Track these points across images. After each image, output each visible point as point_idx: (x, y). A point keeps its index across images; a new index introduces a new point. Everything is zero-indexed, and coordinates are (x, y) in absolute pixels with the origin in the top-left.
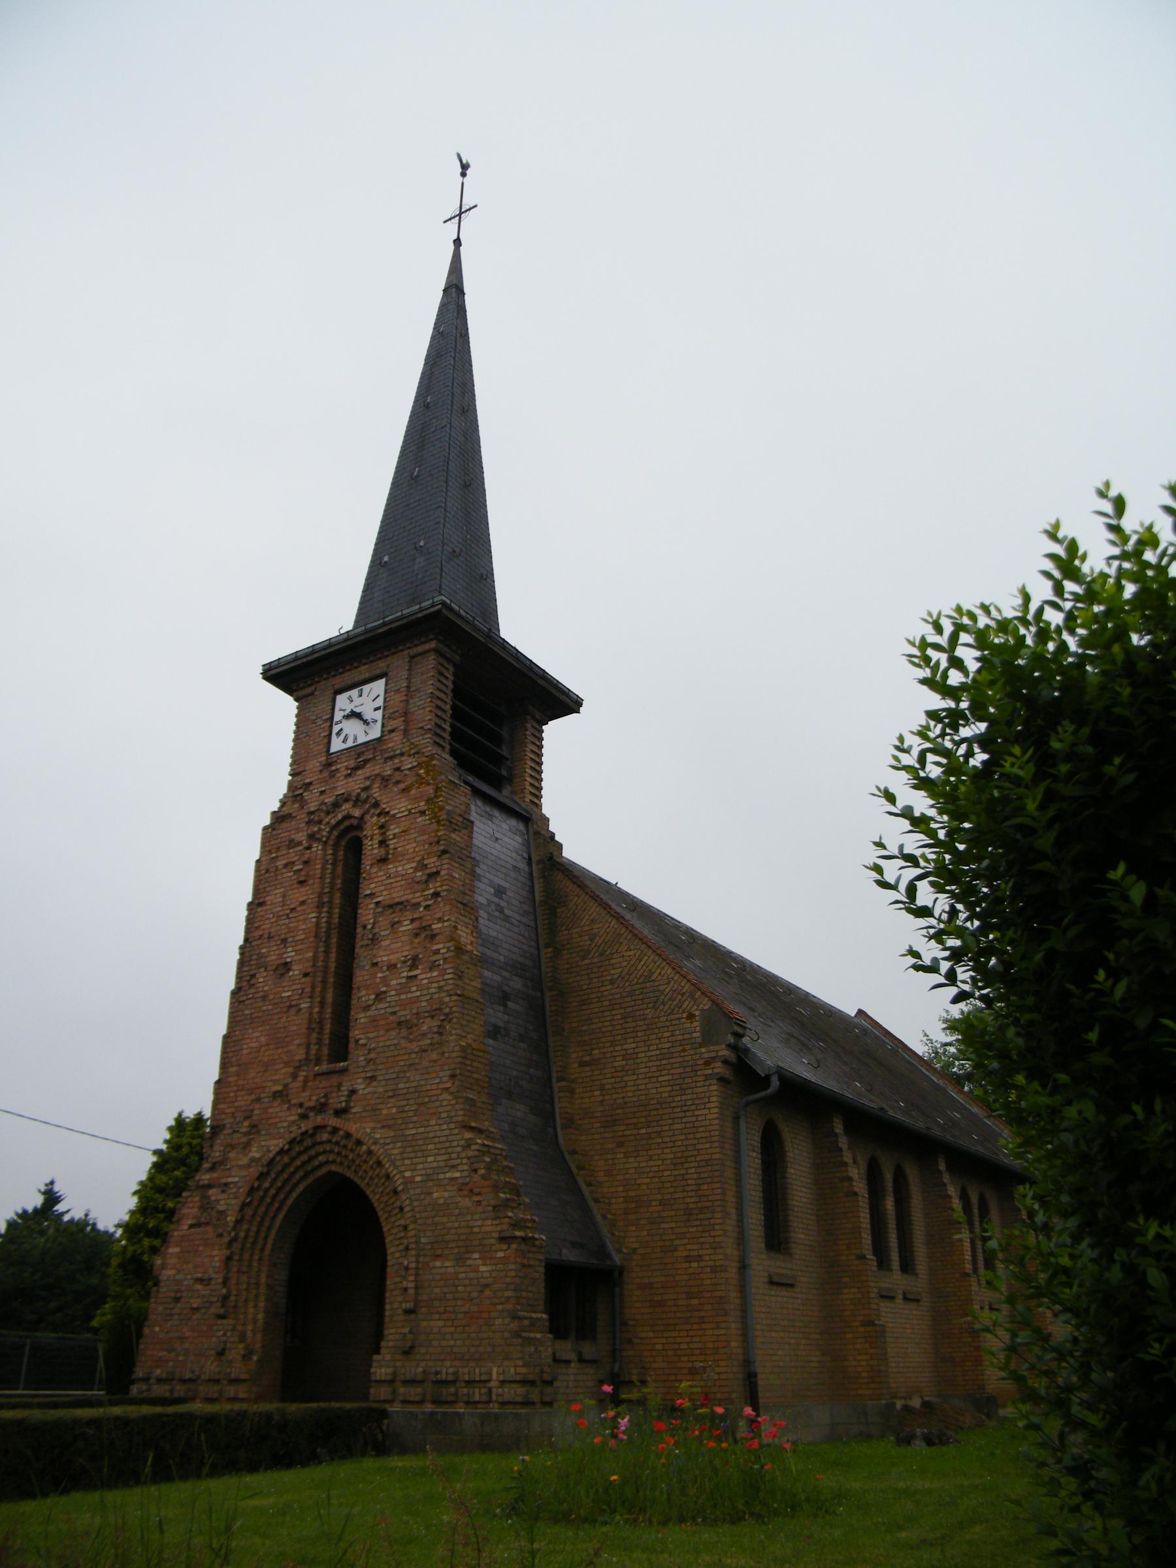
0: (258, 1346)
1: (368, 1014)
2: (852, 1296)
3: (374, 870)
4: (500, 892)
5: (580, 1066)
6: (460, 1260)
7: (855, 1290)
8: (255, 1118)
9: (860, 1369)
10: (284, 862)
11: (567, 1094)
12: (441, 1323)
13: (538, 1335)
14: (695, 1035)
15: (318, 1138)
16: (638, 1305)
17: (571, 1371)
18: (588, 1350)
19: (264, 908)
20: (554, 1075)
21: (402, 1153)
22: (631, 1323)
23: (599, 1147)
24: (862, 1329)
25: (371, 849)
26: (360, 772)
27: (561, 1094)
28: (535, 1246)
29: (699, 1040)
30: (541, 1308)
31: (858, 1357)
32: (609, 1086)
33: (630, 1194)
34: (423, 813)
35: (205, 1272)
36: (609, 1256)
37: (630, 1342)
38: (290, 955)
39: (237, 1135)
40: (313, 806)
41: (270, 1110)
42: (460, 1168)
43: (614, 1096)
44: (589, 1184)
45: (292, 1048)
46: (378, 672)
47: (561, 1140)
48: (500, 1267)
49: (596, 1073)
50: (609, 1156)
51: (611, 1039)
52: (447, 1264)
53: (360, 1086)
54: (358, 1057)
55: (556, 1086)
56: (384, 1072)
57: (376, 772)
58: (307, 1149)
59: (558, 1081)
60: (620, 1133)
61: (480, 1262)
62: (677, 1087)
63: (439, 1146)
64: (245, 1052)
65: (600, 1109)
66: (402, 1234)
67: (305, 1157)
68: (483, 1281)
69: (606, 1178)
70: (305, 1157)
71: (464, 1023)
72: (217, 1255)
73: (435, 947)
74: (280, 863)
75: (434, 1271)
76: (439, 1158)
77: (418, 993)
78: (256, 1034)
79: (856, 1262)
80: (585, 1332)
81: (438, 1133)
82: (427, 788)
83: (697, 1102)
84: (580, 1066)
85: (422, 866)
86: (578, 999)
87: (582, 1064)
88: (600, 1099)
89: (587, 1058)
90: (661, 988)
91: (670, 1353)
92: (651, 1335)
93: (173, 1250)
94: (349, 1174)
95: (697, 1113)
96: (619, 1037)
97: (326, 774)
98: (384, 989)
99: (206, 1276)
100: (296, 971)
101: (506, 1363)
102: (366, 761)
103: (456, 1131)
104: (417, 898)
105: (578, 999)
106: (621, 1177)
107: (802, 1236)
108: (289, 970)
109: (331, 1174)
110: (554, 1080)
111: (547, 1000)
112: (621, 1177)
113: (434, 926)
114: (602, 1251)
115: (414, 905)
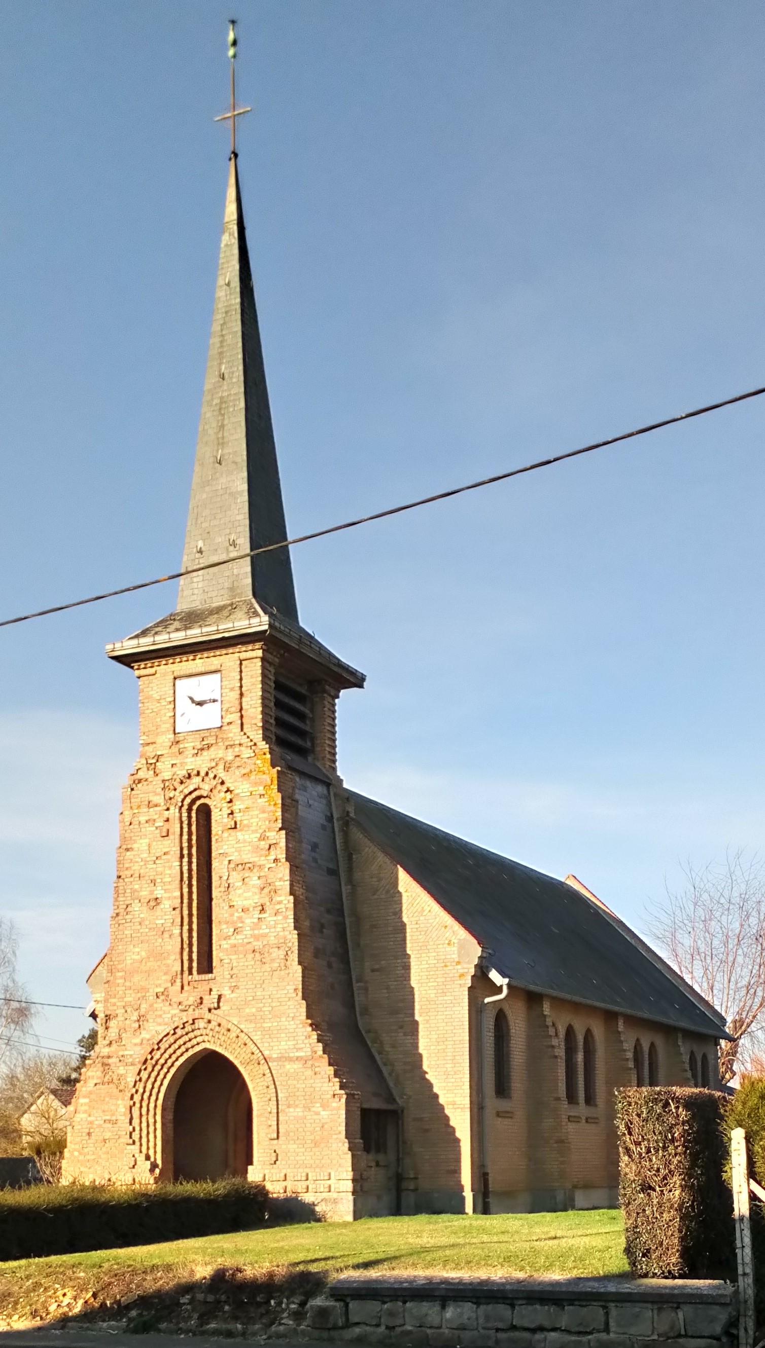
0: (159, 1162)
1: (229, 942)
3: (226, 835)
4: (315, 847)
6: (307, 1108)
10: (147, 818)
12: (295, 1146)
15: (196, 1026)
18: (381, 1157)
19: (133, 853)
20: (354, 977)
24: (555, 1145)
25: (219, 819)
26: (205, 753)
29: (457, 960)
30: (359, 1136)
33: (408, 1060)
34: (261, 796)
35: (113, 1115)
36: (394, 1100)
38: (159, 893)
40: (167, 775)
41: (155, 1005)
44: (380, 1053)
45: (169, 962)
46: (213, 668)
47: (360, 1024)
48: (335, 1112)
52: (298, 1110)
53: (226, 992)
55: (356, 985)
57: (220, 756)
66: (265, 1091)
67: (186, 1038)
68: (323, 1121)
70: (186, 1038)
72: (122, 1106)
73: (279, 899)
74: (143, 819)
76: (289, 1043)
77: (267, 931)
82: (264, 776)
85: (263, 838)
87: (373, 971)
89: (377, 967)
90: (431, 921)
93: (82, 1101)
97: (175, 749)
98: (240, 925)
99: (114, 1118)
100: (166, 905)
101: (340, 1169)
102: (209, 747)
104: (262, 861)
107: (519, 1085)
108: (158, 904)
109: (205, 1049)
110: (354, 982)
113: (277, 884)
114: (391, 1099)
115: (260, 866)
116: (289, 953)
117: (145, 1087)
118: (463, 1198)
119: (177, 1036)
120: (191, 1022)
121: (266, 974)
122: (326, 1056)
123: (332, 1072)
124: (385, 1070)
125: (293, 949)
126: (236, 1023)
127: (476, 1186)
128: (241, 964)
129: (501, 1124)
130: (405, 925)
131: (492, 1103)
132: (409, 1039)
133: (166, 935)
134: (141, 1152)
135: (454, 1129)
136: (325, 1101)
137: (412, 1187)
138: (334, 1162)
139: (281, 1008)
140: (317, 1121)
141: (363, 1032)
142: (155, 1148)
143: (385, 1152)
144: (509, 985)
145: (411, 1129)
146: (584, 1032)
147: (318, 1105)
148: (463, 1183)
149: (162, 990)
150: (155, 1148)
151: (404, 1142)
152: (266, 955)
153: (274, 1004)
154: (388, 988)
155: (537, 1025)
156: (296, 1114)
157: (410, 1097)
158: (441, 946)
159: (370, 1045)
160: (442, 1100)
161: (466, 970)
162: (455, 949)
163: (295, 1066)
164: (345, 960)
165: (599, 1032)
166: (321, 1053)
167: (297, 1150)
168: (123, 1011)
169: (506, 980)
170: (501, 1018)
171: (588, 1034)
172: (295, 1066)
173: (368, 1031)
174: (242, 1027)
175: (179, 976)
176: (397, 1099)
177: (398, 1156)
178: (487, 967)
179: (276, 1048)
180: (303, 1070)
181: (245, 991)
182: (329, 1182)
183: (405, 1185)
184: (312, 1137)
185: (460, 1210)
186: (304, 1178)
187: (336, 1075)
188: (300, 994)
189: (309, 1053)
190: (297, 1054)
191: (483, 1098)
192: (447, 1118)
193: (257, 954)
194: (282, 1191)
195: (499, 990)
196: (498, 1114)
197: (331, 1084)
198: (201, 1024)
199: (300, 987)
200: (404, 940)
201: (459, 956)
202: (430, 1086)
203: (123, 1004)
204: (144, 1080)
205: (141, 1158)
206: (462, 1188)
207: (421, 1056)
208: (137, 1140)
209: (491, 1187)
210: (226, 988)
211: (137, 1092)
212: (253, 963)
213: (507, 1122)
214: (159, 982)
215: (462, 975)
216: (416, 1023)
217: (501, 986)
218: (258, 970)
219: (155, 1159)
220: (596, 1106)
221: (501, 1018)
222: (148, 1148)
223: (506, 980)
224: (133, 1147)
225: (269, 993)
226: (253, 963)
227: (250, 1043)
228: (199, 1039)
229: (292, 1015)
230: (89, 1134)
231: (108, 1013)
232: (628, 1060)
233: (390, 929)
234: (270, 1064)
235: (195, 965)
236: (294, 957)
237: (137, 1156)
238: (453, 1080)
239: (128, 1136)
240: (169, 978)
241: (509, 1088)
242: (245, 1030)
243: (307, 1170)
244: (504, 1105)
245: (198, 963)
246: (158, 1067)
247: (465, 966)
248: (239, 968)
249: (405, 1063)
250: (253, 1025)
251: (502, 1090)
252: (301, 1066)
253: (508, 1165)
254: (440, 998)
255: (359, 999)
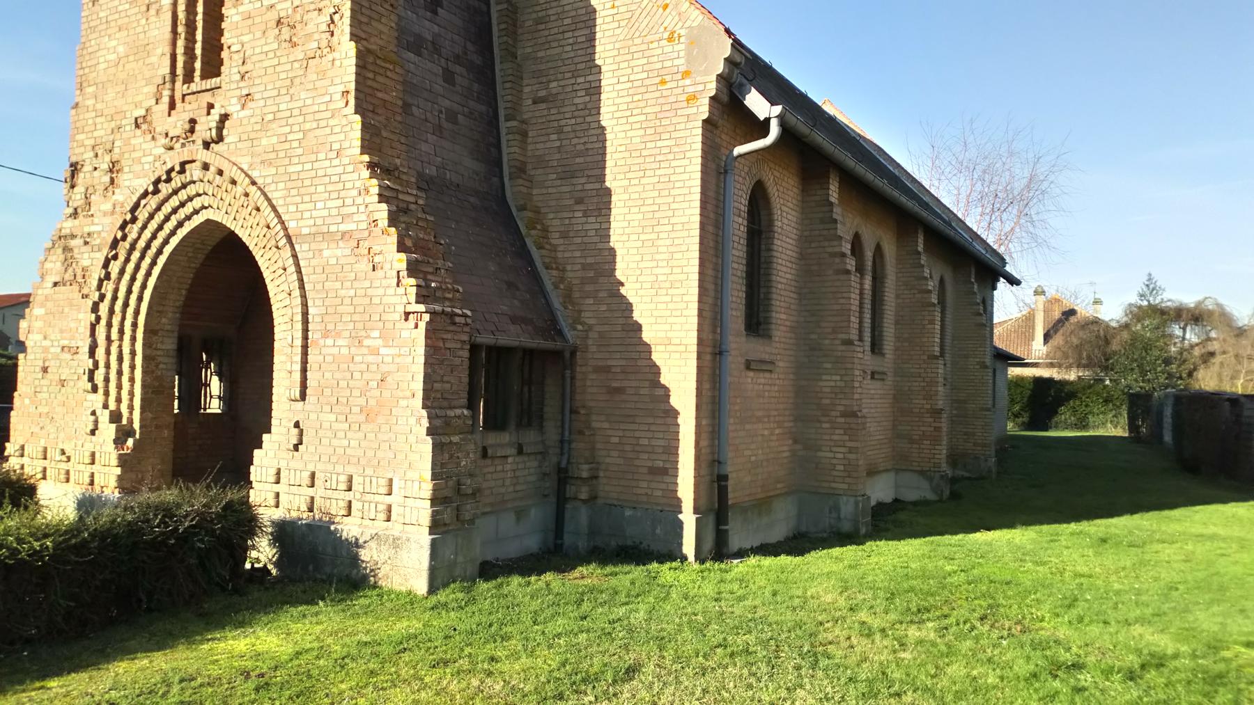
2: (833, 384)
5: (535, 103)
7: (838, 378)
8: (116, 150)
9: (834, 461)
11: (517, 137)
12: (332, 417)
13: (455, 439)
14: (676, 62)
16: (595, 390)
17: (508, 467)
18: (530, 437)
20: (502, 113)
21: (285, 198)
22: (582, 412)
23: (553, 203)
24: (842, 420)
27: (511, 137)
28: (455, 324)
29: (682, 69)
31: (834, 449)
32: (569, 129)
33: (589, 260)
35: (72, 338)
36: (560, 333)
37: (581, 433)
39: (96, 174)
41: (133, 141)
42: (356, 218)
43: (575, 141)
45: (154, 59)
49: (553, 111)
50: (565, 215)
51: (573, 67)
52: (340, 342)
53: (233, 108)
54: (230, 68)
55: (504, 126)
56: (262, 88)
58: (175, 192)
59: (507, 120)
60: (580, 187)
61: (380, 342)
62: (652, 131)
63: (330, 188)
64: (102, 66)
65: (557, 156)
69: (561, 241)
71: (364, 19)
75: (324, 351)
76: (330, 204)
78: (114, 43)
79: (843, 348)
80: (530, 417)
81: (329, 171)
83: (675, 149)
84: (535, 103)
86: (534, 16)
88: (558, 144)
89: (542, 93)
91: (628, 448)
92: (606, 425)
94: (231, 225)
95: (674, 163)
96: (582, 66)
99: (73, 344)
103: (350, 168)
105: (534, 16)
106: (579, 240)
107: (783, 316)
109: (208, 221)
110: (502, 118)
111: (494, 16)
112: (579, 240)
114: (552, 328)
116: (336, 17)
117: (116, 291)
118: (680, 524)
119: (161, 196)
120: (177, 168)
121: (296, 65)
122: (393, 229)
123: (404, 266)
124: (548, 278)
125: (343, 9)
126: (245, 167)
127: (703, 502)
128: (258, 50)
129: (753, 382)
130: (595, 11)
131: (739, 345)
132: (592, 224)
133: (152, 12)
134: (106, 406)
135: (666, 390)
136: (389, 325)
137: (583, 496)
138: (400, 456)
139: (318, 132)
140: (373, 368)
141: (514, 210)
142: (131, 400)
143: (541, 427)
144: (781, 117)
145: (590, 389)
146: (873, 247)
147: (376, 334)
148: (680, 494)
149: (143, 112)
150: (131, 400)
151: (573, 411)
152: (299, 26)
153: (308, 126)
154: (560, 131)
155: (817, 222)
156: (335, 350)
157: (590, 328)
158: (655, 45)
159: (523, 230)
160: (647, 336)
161: (701, 87)
162: (682, 47)
163: (339, 252)
164: (485, 76)
165: (890, 250)
166: (386, 222)
167: (336, 426)
168: (91, 154)
169: (778, 109)
170: (759, 200)
171: (878, 250)
172: (339, 252)
173: (522, 208)
174: (254, 174)
175: (168, 85)
176: (566, 330)
177: (562, 434)
178: (741, 85)
179: (307, 215)
180: (352, 260)
181: (262, 103)
182: (388, 499)
183: (570, 490)
184: (362, 401)
185: (672, 554)
186: (343, 486)
187: (413, 270)
188: (352, 102)
189: (364, 226)
190: (343, 227)
191: (713, 369)
192: (656, 371)
193: (285, 30)
194: (304, 507)
195: (761, 128)
196: (748, 366)
197: (401, 290)
198: (194, 172)
199: (352, 86)
200: (591, 39)
201: (688, 62)
202: (629, 307)
203: (92, 142)
204: (114, 276)
205: (104, 416)
206: (677, 506)
207: (612, 252)
208: (101, 384)
209: (732, 497)
210: (234, 101)
211: (102, 297)
212: (275, 46)
213: (763, 378)
214: (140, 98)
215: (692, 98)
216: (608, 192)
217: (768, 120)
218: (283, 60)
219: (131, 421)
220: (883, 355)
221: (759, 200)
222: (119, 400)
223: (778, 109)
224: (92, 396)
225: (300, 104)
226: (275, 46)
227: (264, 205)
228: (197, 203)
229: (336, 146)
230: (45, 370)
231: (74, 159)
232: (930, 292)
233: (567, 21)
234: (297, 247)
235: (198, 65)
236: (344, 26)
237: (98, 413)
238: (668, 299)
239: (86, 377)
240: (153, 89)
241: (767, 321)
242: (260, 181)
243: (350, 470)
244: (757, 349)
245: (202, 62)
246: (136, 255)
247: (699, 79)
248: (255, 58)
249: (585, 267)
250: (273, 171)
251: (756, 323)
252: (348, 252)
253: (759, 452)
254: (649, 145)
255: (510, 150)
